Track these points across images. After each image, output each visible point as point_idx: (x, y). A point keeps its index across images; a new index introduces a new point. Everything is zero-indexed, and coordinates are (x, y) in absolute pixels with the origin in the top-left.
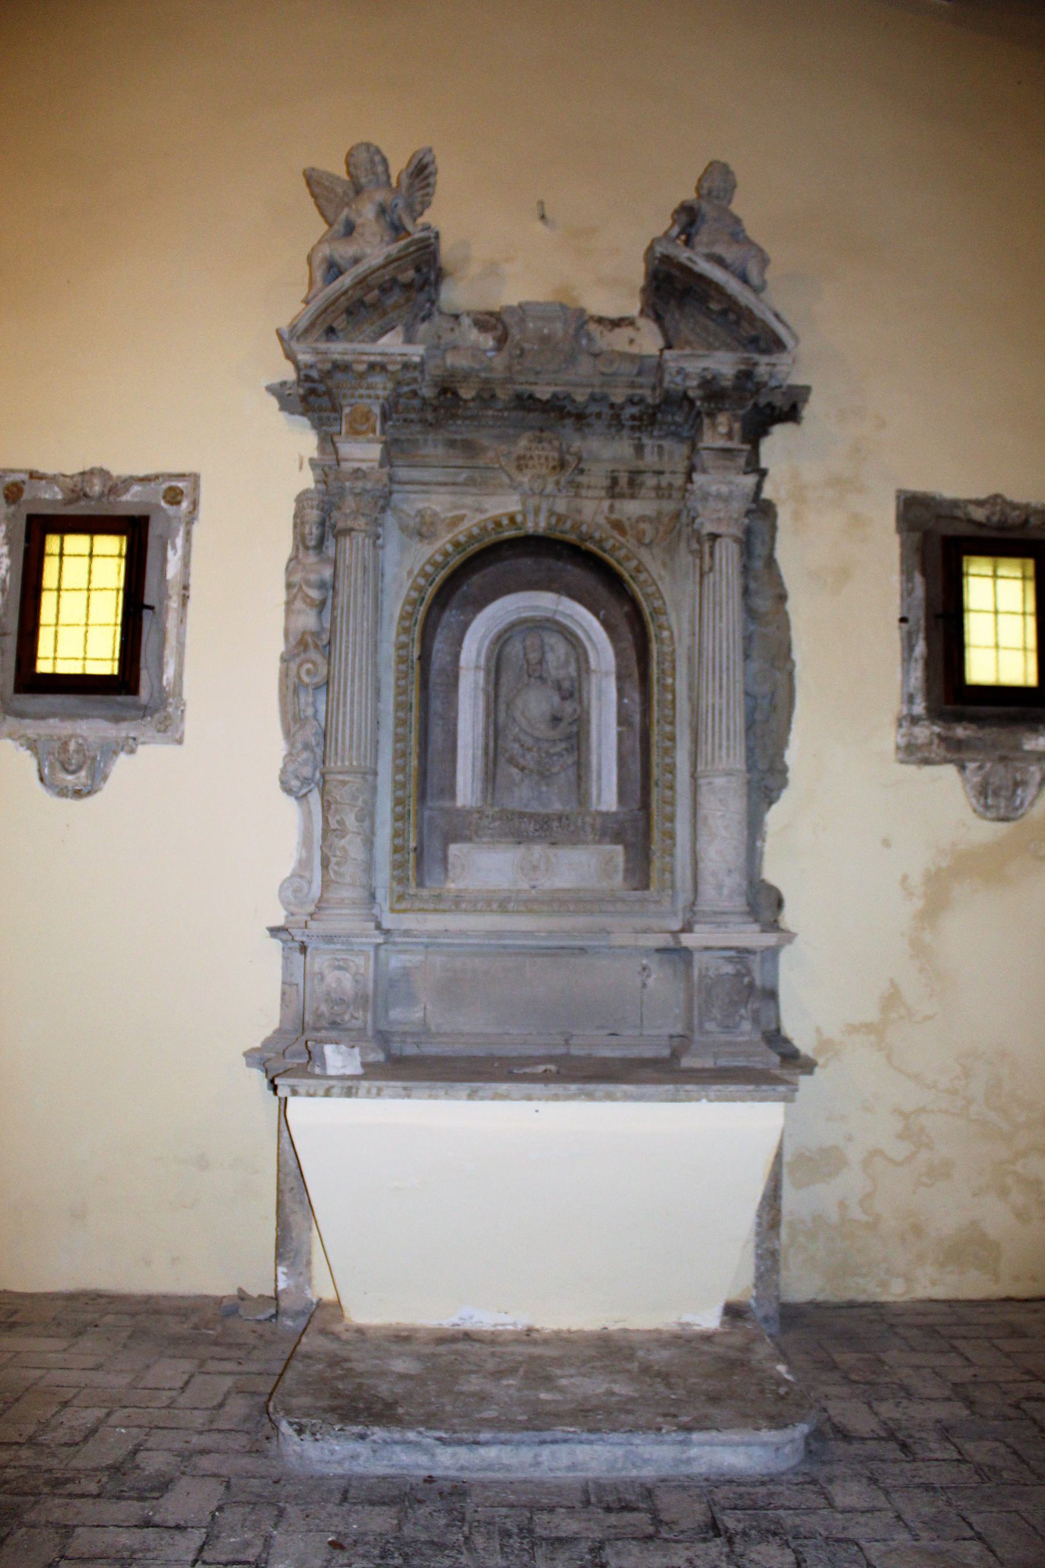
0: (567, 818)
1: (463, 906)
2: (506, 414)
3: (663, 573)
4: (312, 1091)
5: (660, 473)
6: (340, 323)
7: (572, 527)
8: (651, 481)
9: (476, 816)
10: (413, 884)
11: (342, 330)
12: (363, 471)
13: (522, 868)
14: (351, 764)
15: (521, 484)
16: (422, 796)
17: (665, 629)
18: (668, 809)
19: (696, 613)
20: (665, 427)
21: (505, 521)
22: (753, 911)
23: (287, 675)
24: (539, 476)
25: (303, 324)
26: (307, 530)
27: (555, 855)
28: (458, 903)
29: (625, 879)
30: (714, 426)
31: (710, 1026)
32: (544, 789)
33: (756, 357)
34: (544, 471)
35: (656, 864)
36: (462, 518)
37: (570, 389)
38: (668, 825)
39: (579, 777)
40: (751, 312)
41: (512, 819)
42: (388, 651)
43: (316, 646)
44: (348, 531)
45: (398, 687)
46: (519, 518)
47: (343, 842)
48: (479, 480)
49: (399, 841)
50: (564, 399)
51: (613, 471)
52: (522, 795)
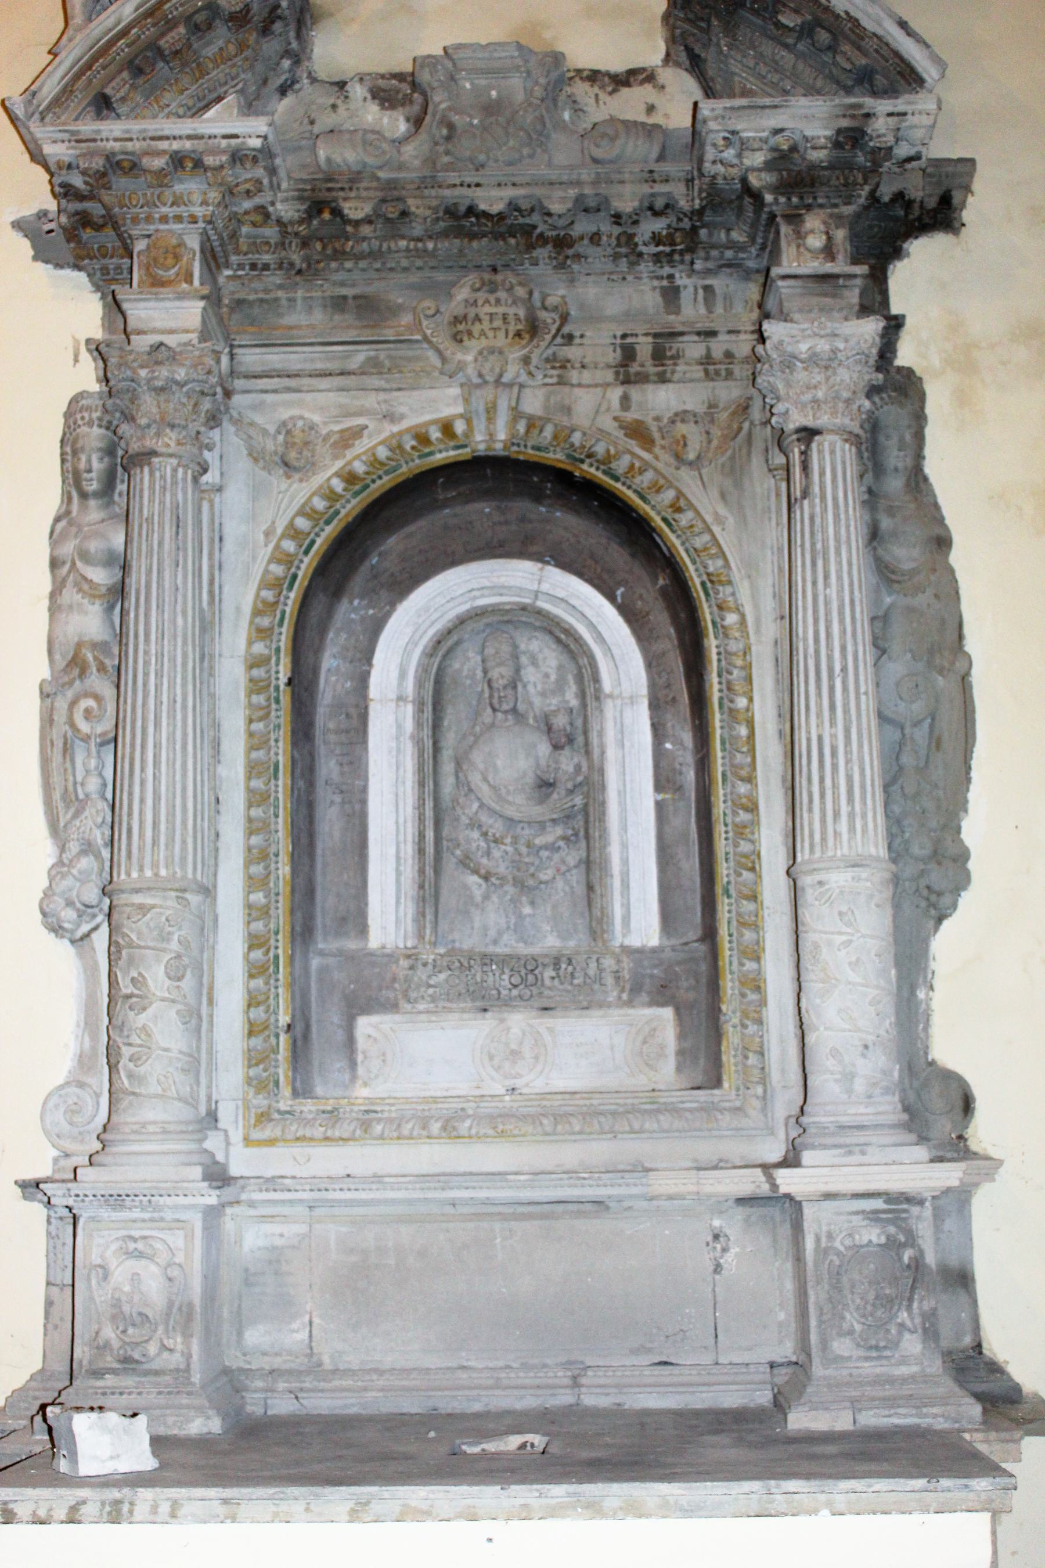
0: (570, 962)
1: (378, 1129)
2: (430, 245)
3: (722, 510)
4: (42, 1513)
5: (712, 334)
6: (115, 90)
7: (555, 437)
8: (693, 349)
9: (404, 963)
10: (286, 1091)
11: (123, 99)
12: (169, 348)
13: (491, 1057)
14: (156, 875)
15: (461, 366)
16: (303, 933)
17: (730, 610)
18: (749, 935)
19: (785, 576)
20: (714, 253)
21: (435, 434)
22: (915, 1121)
23: (51, 721)
24: (492, 351)
25: (50, 88)
26: (82, 465)
27: (551, 1030)
28: (368, 1123)
29: (679, 1069)
30: (800, 236)
31: (842, 1347)
32: (527, 910)
33: (869, 102)
34: (501, 341)
35: (732, 1038)
36: (358, 432)
37: (539, 192)
38: (750, 966)
39: (590, 888)
40: (856, 22)
41: (470, 967)
42: (232, 673)
43: (102, 668)
44: (146, 456)
45: (251, 735)
46: (460, 427)
47: (142, 1019)
48: (387, 363)
49: (258, 1014)
50: (532, 210)
51: (624, 336)
52: (488, 924)
